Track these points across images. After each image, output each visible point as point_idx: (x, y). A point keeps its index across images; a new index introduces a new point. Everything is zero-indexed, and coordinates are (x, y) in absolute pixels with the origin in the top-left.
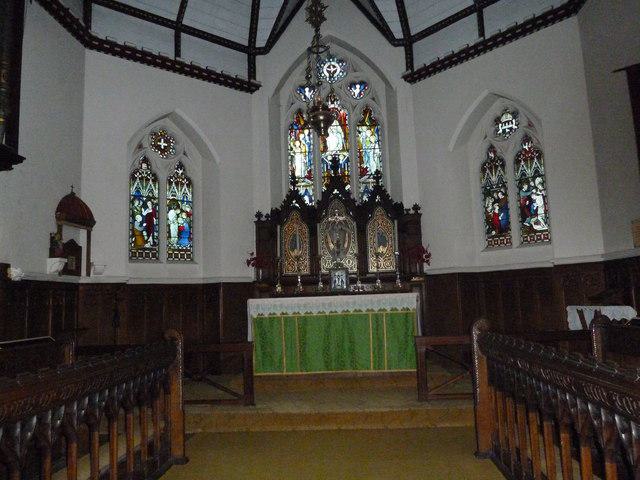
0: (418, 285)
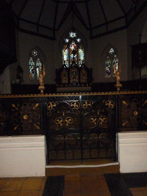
0: (91, 85)
